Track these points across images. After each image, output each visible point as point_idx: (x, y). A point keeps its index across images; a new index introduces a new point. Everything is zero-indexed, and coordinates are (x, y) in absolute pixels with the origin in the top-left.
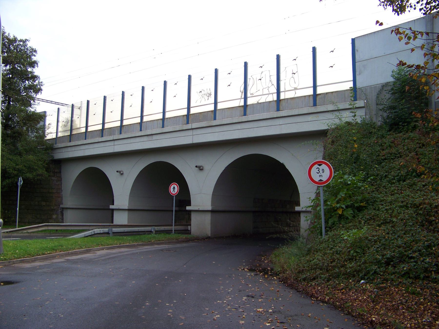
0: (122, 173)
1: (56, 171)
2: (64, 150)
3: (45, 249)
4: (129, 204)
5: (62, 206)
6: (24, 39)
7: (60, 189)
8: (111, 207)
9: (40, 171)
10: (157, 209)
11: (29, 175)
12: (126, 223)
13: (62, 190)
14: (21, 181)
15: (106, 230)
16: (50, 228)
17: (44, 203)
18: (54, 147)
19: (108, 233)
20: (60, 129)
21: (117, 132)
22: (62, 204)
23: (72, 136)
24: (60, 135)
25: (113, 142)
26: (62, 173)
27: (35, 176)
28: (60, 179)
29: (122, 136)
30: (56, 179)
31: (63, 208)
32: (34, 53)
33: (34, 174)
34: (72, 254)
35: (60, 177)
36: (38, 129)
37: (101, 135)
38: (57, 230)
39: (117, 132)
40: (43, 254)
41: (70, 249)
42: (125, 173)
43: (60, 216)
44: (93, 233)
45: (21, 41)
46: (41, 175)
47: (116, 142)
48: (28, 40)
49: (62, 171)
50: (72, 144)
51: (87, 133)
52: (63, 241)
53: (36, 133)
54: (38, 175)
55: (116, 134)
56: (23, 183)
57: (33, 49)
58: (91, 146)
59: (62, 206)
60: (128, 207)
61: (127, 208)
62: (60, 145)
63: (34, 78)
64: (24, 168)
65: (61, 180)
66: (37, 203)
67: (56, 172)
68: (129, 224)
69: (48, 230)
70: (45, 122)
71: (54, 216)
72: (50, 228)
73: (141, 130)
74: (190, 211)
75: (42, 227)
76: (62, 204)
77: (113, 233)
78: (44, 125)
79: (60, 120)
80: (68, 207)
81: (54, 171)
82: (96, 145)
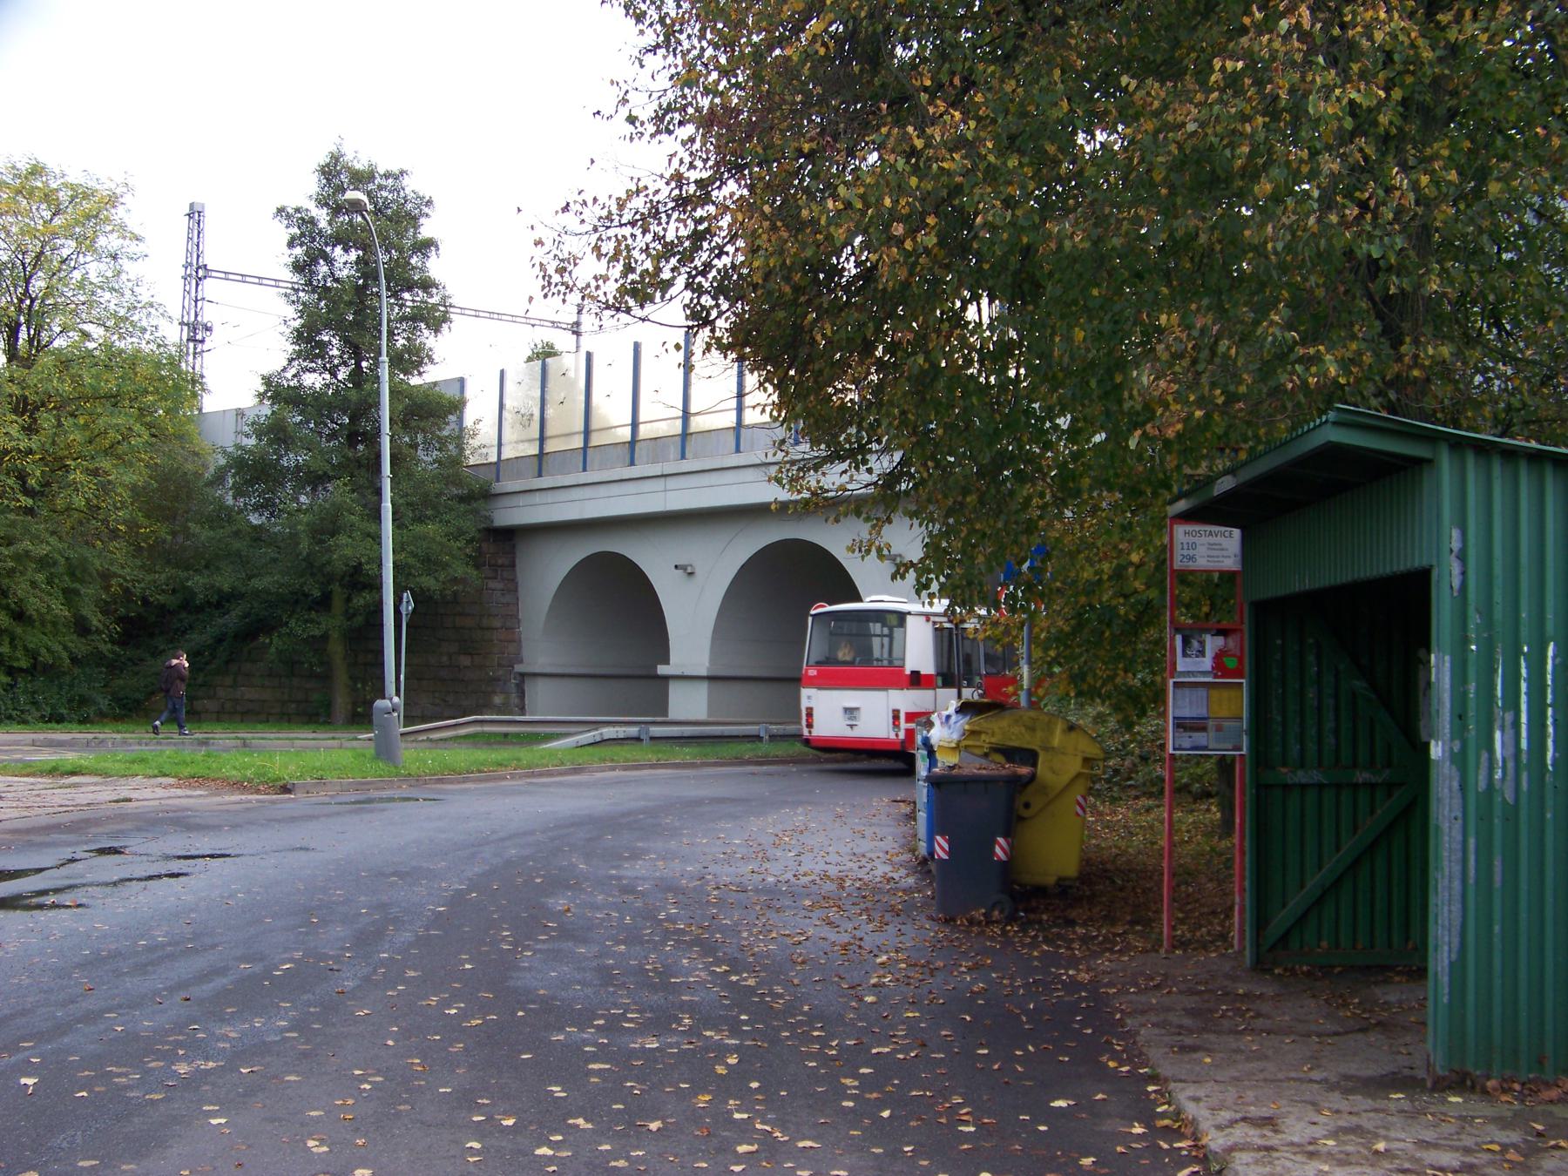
0: (689, 570)
1: (500, 562)
2: (522, 500)
3: (482, 764)
4: (712, 660)
5: (518, 668)
6: (395, 169)
7: (515, 617)
8: (662, 670)
9: (460, 570)
10: (630, 672)
11: (428, 582)
12: (702, 715)
13: (519, 621)
14: (408, 602)
15: (633, 731)
16: (487, 729)
17: (465, 661)
18: (493, 492)
19: (638, 739)
20: (508, 435)
21: (674, 451)
22: (521, 661)
23: (545, 457)
24: (508, 453)
25: (663, 479)
26: (518, 568)
27: (444, 583)
28: (512, 587)
29: (686, 466)
30: (500, 586)
31: (523, 675)
32: (426, 210)
33: (442, 577)
34: (541, 775)
35: (513, 580)
36: (443, 442)
37: (628, 461)
38: (506, 735)
39: (672, 449)
40: (480, 771)
41: (537, 766)
42: (698, 571)
43: (514, 699)
44: (598, 739)
45: (387, 176)
46: (463, 581)
47: (671, 483)
48: (406, 172)
49: (517, 561)
50: (546, 482)
51: (590, 452)
52: (525, 754)
53: (440, 450)
54: (455, 580)
55: (672, 457)
56: (414, 609)
57: (422, 198)
58: (602, 490)
59: (518, 668)
60: (708, 669)
61: (704, 673)
62: (508, 485)
63: (427, 285)
64: (411, 561)
65: (516, 590)
66: (445, 659)
67: (502, 566)
68: (711, 719)
69: (483, 733)
70: (460, 419)
71: (497, 700)
72: (487, 729)
73: (738, 450)
74: (667, 678)
75: (467, 725)
76: (521, 661)
77: (652, 738)
78: (462, 429)
79: (508, 403)
80: (537, 670)
81: (493, 562)
82: (615, 489)
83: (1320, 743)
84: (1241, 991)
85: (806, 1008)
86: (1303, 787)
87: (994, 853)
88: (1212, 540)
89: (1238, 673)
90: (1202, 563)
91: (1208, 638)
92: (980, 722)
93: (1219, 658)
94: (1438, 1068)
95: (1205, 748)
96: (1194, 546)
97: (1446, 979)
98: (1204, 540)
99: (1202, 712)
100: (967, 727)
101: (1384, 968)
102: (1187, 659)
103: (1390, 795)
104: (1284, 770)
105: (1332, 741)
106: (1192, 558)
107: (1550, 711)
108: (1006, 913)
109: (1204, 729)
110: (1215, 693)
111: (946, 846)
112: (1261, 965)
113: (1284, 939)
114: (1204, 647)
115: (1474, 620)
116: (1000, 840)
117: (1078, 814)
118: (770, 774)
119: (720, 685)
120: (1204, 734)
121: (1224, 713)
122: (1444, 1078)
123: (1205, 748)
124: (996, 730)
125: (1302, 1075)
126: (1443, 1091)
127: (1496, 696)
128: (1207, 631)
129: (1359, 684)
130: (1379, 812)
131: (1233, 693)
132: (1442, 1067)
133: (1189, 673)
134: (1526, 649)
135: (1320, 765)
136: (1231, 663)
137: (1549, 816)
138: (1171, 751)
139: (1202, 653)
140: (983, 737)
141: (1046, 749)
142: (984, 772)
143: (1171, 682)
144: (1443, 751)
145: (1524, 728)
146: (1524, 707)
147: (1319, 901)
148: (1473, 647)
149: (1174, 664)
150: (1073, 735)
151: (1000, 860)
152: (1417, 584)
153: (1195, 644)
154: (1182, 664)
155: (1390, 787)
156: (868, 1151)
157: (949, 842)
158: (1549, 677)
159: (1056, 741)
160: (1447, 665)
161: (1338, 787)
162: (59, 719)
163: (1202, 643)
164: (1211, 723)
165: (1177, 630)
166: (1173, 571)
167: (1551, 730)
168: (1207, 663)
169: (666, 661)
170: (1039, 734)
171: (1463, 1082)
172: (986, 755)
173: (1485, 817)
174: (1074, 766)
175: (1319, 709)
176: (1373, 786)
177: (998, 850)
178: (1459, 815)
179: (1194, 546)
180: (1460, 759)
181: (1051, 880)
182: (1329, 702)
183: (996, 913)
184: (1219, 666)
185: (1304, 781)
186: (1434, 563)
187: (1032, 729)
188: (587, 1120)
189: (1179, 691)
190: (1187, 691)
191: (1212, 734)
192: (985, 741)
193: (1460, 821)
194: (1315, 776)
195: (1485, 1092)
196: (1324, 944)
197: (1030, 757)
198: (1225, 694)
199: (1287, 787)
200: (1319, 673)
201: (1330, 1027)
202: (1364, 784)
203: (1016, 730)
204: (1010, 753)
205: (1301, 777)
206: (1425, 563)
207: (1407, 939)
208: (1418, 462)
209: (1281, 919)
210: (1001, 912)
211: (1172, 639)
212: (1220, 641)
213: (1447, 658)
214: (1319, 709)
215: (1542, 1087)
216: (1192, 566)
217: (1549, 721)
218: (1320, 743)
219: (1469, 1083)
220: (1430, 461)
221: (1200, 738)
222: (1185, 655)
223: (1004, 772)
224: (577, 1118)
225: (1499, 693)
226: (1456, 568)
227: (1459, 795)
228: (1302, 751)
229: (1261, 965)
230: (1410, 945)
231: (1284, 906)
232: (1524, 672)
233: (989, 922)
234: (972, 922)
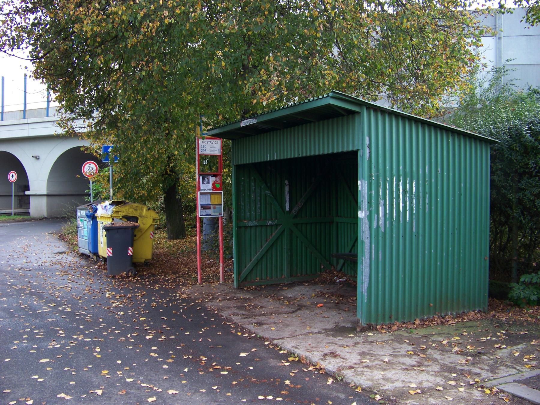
8: (27, 193)
61: (45, 193)
74: (29, 196)
83: (255, 212)
84: (242, 297)
85: (101, 320)
86: (251, 227)
87: (128, 253)
88: (211, 144)
89: (220, 189)
90: (208, 152)
91: (210, 177)
92: (119, 208)
93: (214, 184)
94: (363, 324)
95: (210, 215)
96: (205, 147)
97: (366, 294)
98: (209, 144)
99: (209, 203)
100: (114, 210)
101: (277, 285)
102: (204, 185)
103: (277, 229)
104: (245, 222)
105: (259, 211)
106: (205, 151)
107: (394, 200)
108: (133, 273)
109: (210, 208)
110: (213, 196)
111: (111, 251)
112: (240, 288)
113: (246, 278)
114: (209, 181)
115: (373, 170)
116: (130, 248)
117: (151, 238)
118: (7, 226)
119: (50, 198)
120: (210, 210)
121: (216, 203)
122: (365, 327)
123: (210, 215)
124: (124, 210)
125: (307, 331)
126: (365, 331)
127: (380, 195)
128: (210, 175)
129: (268, 192)
130: (274, 234)
131: (219, 196)
132: (364, 324)
133: (204, 189)
134: (388, 179)
135: (256, 220)
136: (218, 186)
137: (394, 235)
138: (199, 216)
139: (208, 183)
140: (120, 213)
141: (141, 217)
142: (124, 225)
143: (199, 193)
144: (365, 215)
145: (387, 206)
146: (387, 199)
147: (256, 265)
148: (374, 178)
149: (200, 187)
150: (150, 211)
151: (130, 255)
152: (354, 155)
153: (206, 180)
154: (202, 187)
155: (277, 225)
156: (199, 392)
157: (112, 250)
158: (394, 188)
159: (144, 214)
160: (366, 184)
161: (261, 226)
162: (356, 306)
163: (208, 179)
164: (212, 206)
165: (201, 175)
166: (199, 155)
167: (395, 206)
168: (210, 186)
169: (29, 190)
170: (138, 211)
171: (370, 327)
172: (121, 219)
173: (377, 237)
174: (150, 222)
175: (255, 200)
176: (272, 225)
177: (129, 251)
178: (369, 237)
179: (205, 147)
180: (370, 218)
181: (143, 261)
182: (258, 198)
183: (130, 273)
184: (214, 187)
185: (251, 225)
186: (360, 148)
187: (136, 210)
188: (67, 394)
189: (201, 196)
190: (204, 196)
191: (212, 210)
192: (121, 214)
193: (369, 239)
194: (255, 223)
195: (376, 330)
196: (258, 278)
197: (136, 219)
198: (216, 196)
199: (246, 227)
200: (255, 189)
201: (289, 309)
202: (269, 225)
203: (131, 210)
204: (129, 218)
205: (251, 223)
206: (355, 149)
207: (282, 275)
208: (353, 113)
209: (245, 271)
210: (131, 273)
211: (199, 178)
212: (214, 178)
213: (366, 182)
214: (255, 200)
215: (391, 326)
216: (205, 153)
217: (394, 203)
218: (255, 212)
219: (372, 328)
220: (358, 113)
221: (208, 211)
222: (203, 183)
223: (131, 225)
224: (61, 393)
225: (381, 194)
226: (367, 150)
227: (369, 230)
228: (250, 215)
229: (240, 288)
230: (283, 277)
231: (245, 267)
232: (387, 187)
233: (128, 277)
234: (123, 277)
